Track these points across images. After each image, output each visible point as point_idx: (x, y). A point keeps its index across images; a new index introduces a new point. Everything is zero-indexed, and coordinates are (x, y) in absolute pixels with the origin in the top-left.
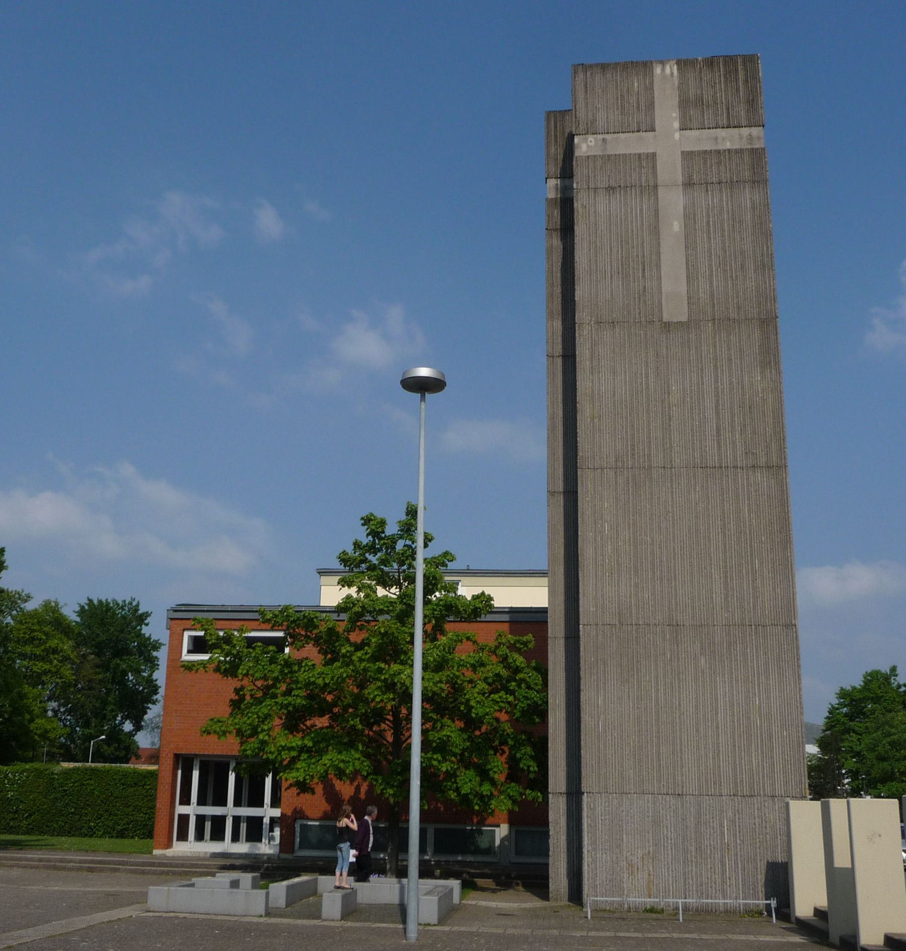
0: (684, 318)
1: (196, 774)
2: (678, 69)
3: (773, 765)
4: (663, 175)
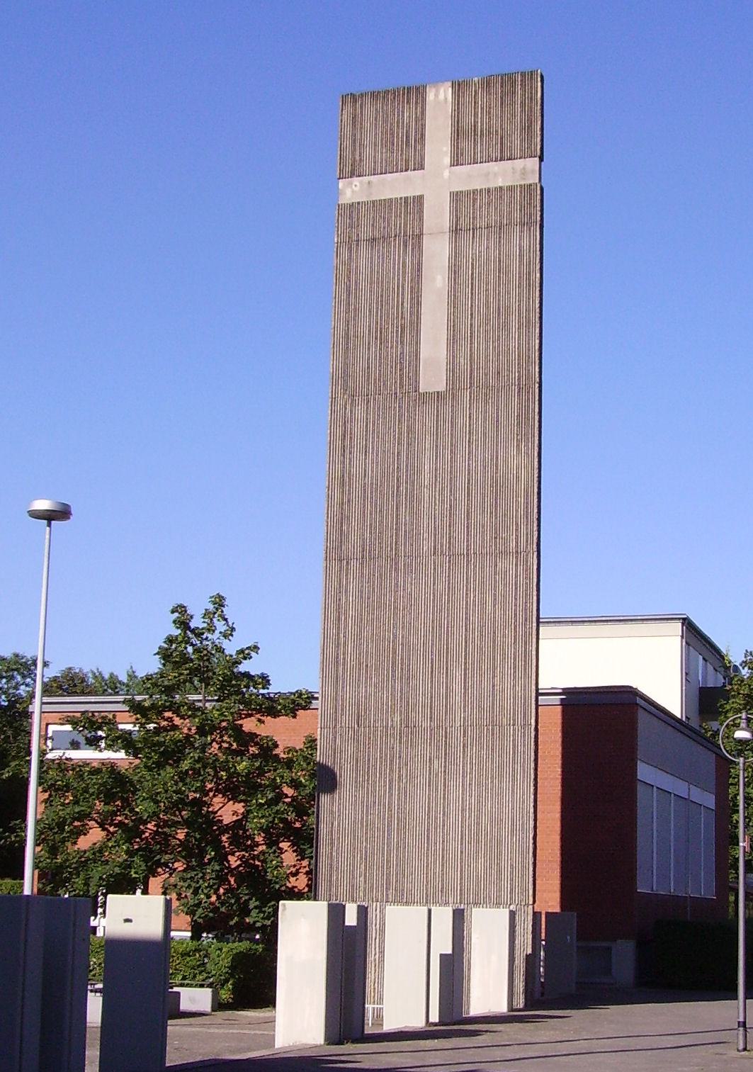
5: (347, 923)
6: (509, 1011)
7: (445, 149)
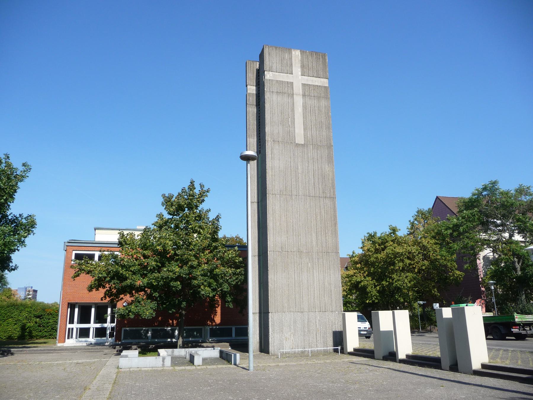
0: (303, 143)
1: (77, 310)
2: (301, 54)
3: (332, 301)
4: (295, 91)
6: (490, 362)
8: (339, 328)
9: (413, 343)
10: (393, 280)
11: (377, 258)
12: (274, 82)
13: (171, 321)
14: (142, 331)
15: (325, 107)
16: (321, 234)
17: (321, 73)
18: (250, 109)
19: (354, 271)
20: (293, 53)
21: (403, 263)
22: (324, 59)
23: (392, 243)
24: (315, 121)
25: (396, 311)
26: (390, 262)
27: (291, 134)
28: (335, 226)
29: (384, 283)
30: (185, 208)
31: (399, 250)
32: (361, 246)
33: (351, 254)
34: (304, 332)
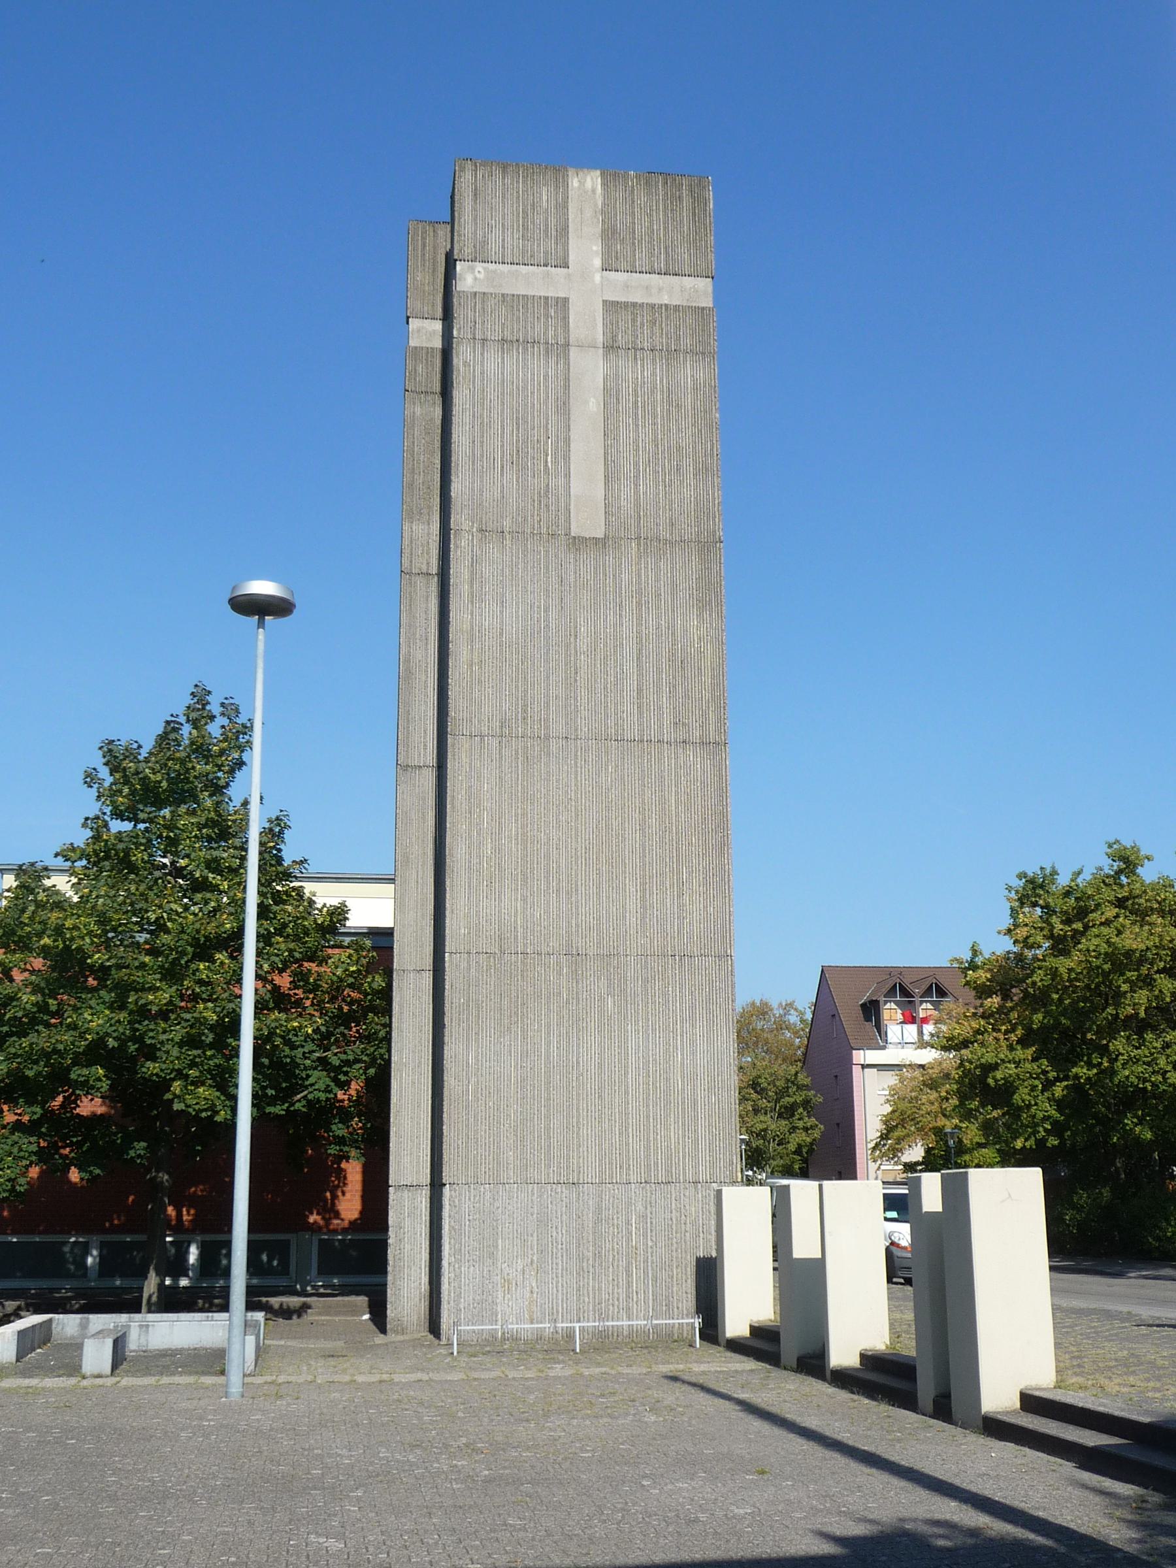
0: (600, 534)
5: (797, 1254)
6: (1058, 1386)
7: (595, 248)
8: (706, 1249)
9: (1055, 1309)
10: (1113, 1061)
11: (1054, 973)
12: (491, 303)
13: (170, 1210)
14: (66, 1249)
15: (695, 389)
16: (663, 883)
17: (683, 254)
18: (418, 411)
19: (975, 1025)
20: (574, 182)
21: (1151, 990)
22: (699, 200)
23: (1111, 912)
24: (652, 447)
25: (826, 1183)
26: (1100, 988)
27: (552, 499)
28: (722, 854)
29: (1081, 1070)
30: (172, 791)
31: (1133, 939)
32: (1007, 922)
33: (967, 956)
34: (581, 1258)
